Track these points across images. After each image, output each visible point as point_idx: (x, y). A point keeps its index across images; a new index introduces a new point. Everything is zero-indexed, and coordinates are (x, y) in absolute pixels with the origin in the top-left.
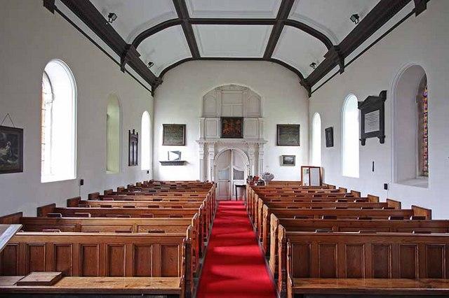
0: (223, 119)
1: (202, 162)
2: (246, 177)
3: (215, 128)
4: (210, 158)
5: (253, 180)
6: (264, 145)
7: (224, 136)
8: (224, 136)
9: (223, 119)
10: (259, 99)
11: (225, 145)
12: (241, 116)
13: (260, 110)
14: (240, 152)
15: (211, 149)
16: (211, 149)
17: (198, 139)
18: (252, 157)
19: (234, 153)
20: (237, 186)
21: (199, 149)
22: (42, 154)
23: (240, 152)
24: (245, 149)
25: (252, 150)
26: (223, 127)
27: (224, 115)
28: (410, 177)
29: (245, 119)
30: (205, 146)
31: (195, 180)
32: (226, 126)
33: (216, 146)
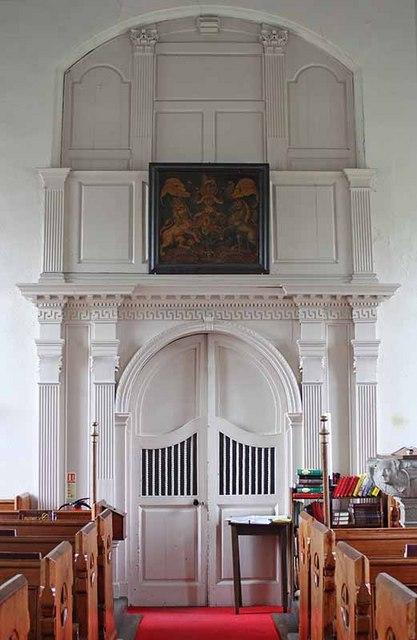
0: (161, 174)
1: (56, 398)
2: (286, 480)
3: (118, 237)
4: (96, 375)
5: (322, 491)
6: (380, 310)
7: (168, 259)
8: (168, 259)
9: (161, 174)
10: (345, 83)
11: (170, 307)
12: (253, 158)
13: (350, 133)
14: (256, 337)
15: (101, 333)
16: (101, 333)
17: (35, 279)
18: (319, 373)
19: (221, 350)
20: (239, 529)
21: (36, 331)
22: (97, 619)
23: (256, 337)
24: (280, 331)
25: (317, 333)
26: (162, 211)
27: (170, 156)
28: (210, 596)
29: (275, 177)
30: (71, 313)
31: (11, 496)
32: (179, 211)
33: (128, 309)
